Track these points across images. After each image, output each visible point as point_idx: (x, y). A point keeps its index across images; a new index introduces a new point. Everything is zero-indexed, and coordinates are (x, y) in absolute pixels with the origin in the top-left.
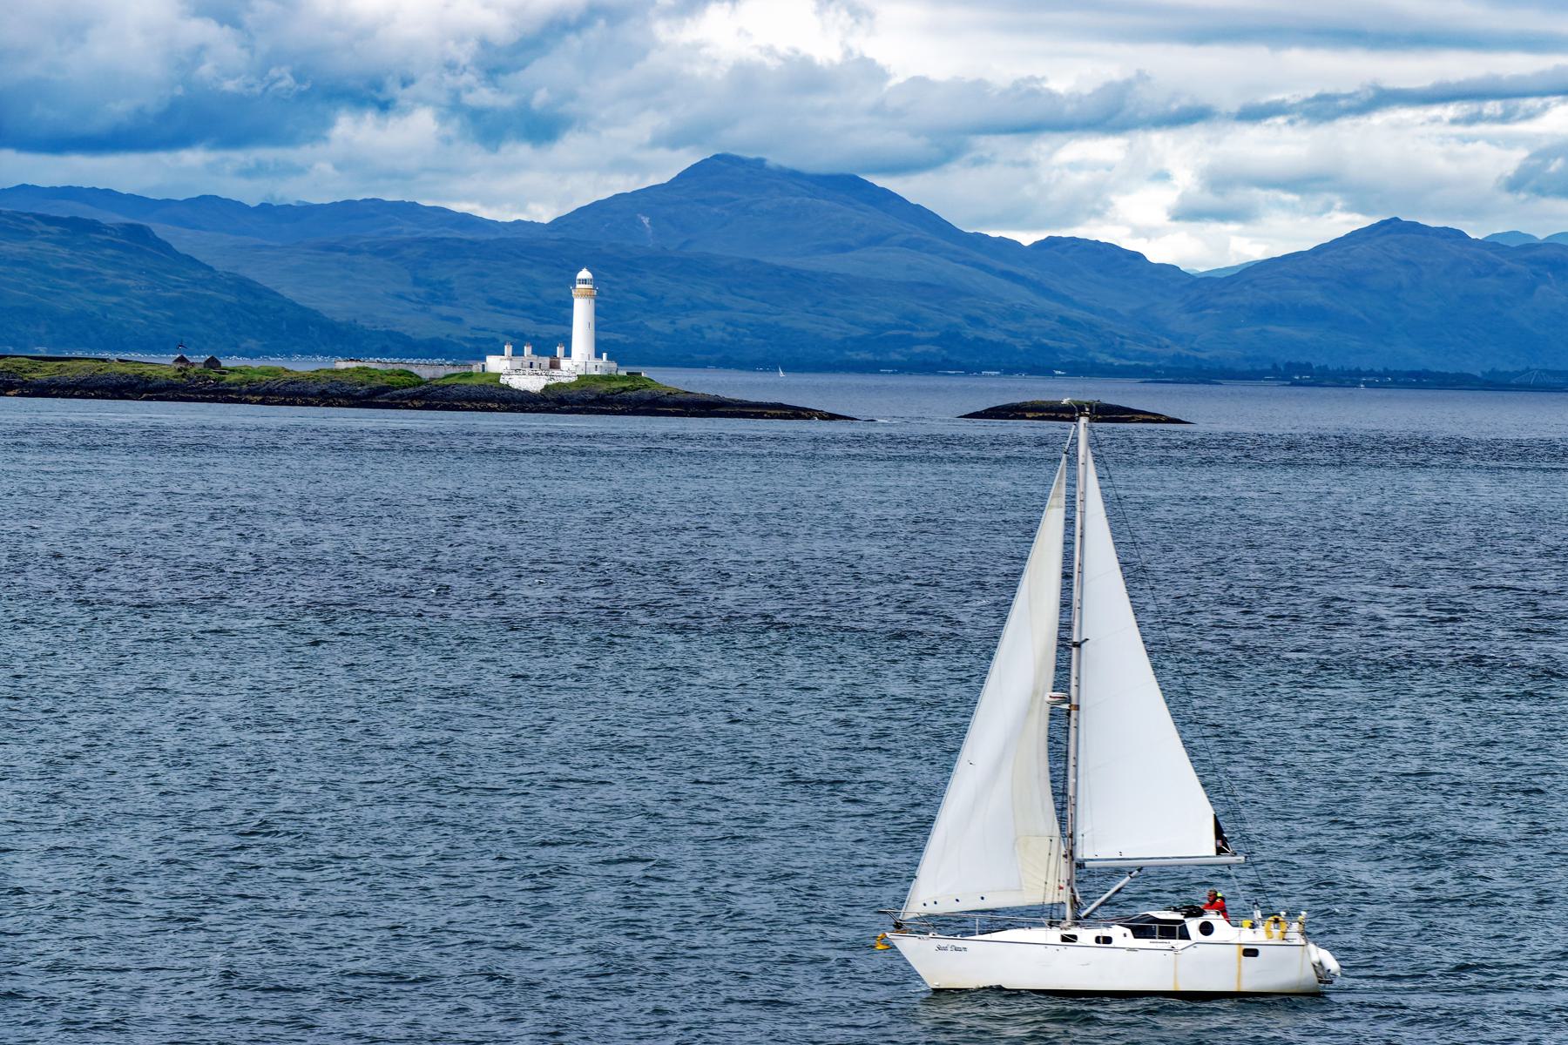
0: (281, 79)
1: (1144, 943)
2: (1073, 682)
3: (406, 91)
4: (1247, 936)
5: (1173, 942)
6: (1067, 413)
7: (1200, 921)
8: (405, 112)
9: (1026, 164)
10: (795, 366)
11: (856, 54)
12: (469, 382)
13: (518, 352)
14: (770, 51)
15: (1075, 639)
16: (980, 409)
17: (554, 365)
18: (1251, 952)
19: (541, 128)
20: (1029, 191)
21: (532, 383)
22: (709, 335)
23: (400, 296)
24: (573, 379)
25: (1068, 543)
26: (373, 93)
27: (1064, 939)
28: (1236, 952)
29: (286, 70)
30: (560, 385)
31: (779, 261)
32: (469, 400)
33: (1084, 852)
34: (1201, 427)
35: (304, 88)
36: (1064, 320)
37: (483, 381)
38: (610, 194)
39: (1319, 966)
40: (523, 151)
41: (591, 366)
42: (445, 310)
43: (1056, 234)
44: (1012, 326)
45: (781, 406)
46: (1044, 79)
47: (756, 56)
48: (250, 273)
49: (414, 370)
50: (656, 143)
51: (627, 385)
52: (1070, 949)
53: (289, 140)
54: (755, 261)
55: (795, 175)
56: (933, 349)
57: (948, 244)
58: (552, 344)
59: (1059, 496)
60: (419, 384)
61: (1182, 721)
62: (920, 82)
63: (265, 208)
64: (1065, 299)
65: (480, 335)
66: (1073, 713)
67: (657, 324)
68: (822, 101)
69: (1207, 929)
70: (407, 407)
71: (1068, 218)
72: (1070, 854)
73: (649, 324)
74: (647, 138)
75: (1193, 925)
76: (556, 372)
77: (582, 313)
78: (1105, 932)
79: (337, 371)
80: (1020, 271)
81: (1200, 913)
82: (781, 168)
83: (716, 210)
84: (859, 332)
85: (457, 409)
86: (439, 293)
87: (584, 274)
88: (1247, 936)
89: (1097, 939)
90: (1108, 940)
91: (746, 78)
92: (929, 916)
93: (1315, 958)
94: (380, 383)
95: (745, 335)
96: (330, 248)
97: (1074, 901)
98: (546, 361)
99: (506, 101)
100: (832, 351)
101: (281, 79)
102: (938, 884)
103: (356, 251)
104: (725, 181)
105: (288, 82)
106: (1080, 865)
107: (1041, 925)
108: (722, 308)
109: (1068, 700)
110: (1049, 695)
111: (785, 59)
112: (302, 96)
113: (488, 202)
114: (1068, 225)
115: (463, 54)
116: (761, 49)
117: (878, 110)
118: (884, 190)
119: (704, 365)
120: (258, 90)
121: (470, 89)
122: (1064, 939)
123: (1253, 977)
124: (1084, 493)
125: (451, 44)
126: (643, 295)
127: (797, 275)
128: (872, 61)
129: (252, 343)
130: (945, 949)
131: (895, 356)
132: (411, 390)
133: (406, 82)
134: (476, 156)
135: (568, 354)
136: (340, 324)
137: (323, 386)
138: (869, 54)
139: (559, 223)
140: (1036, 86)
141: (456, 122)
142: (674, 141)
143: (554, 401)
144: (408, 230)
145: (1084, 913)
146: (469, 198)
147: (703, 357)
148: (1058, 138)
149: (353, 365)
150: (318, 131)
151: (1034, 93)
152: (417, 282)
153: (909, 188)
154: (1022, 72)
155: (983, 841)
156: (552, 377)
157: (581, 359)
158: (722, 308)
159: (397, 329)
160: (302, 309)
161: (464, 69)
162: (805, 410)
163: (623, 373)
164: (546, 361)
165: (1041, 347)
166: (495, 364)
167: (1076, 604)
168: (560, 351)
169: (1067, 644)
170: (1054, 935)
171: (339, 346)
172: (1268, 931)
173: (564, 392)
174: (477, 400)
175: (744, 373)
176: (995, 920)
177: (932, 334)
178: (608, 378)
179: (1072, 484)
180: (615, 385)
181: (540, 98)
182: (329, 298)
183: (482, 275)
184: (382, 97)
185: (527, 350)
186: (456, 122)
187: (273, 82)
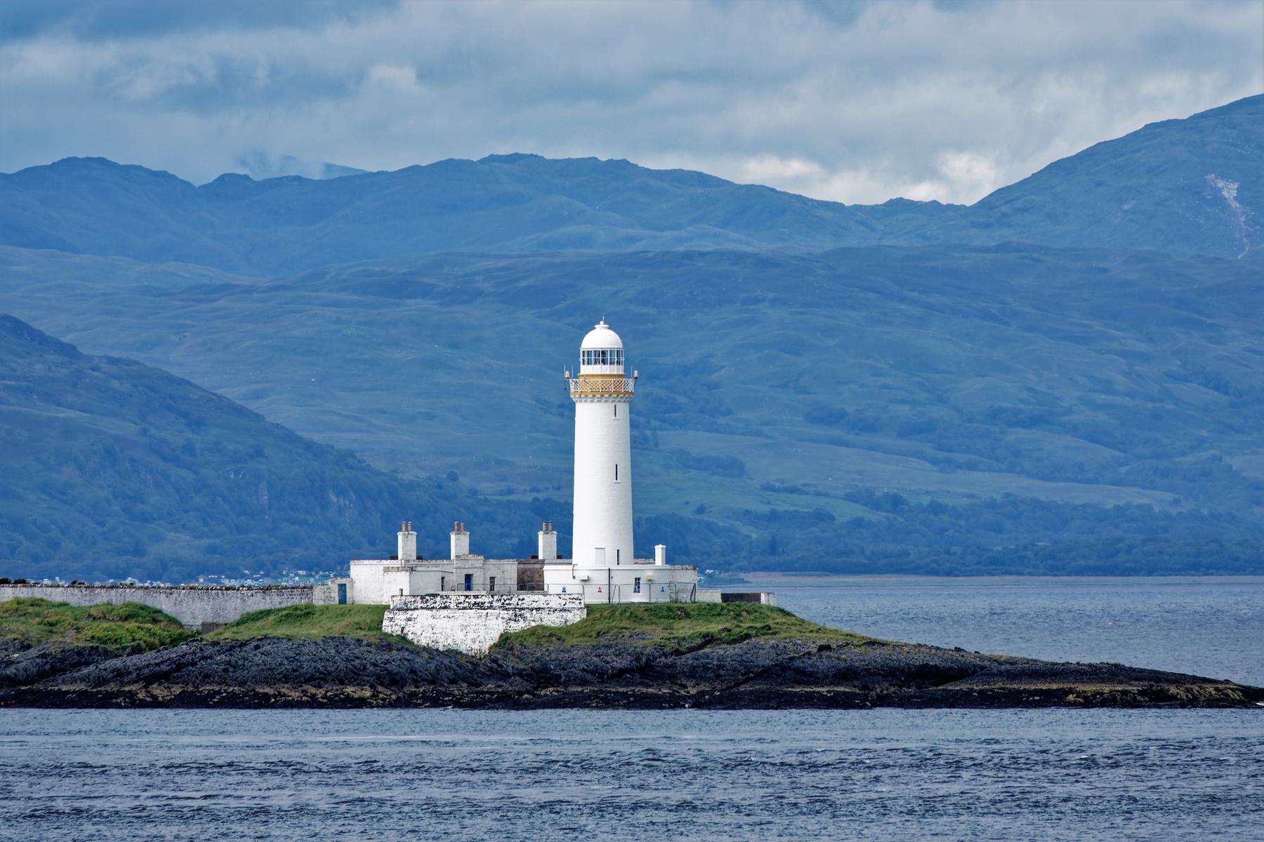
12: (301, 631)
13: (432, 550)
17: (530, 582)
21: (468, 630)
24: (575, 617)
37: (337, 627)
41: (624, 579)
45: (1115, 672)
48: (182, 360)
49: (164, 603)
51: (714, 627)
58: (529, 520)
60: (174, 642)
65: (782, 504)
70: (134, 703)
73: (1236, 462)
76: (530, 599)
77: (597, 435)
85: (262, 702)
87: (601, 337)
94: (72, 640)
98: (509, 570)
126: (1218, 384)
132: (149, 657)
135: (564, 553)
136: (411, 486)
139: (1002, 204)
143: (522, 677)
156: (518, 614)
157: (595, 562)
162: (1179, 679)
163: (714, 596)
164: (509, 570)
166: (373, 581)
168: (545, 543)
173: (549, 653)
174: (317, 678)
180: (686, 629)
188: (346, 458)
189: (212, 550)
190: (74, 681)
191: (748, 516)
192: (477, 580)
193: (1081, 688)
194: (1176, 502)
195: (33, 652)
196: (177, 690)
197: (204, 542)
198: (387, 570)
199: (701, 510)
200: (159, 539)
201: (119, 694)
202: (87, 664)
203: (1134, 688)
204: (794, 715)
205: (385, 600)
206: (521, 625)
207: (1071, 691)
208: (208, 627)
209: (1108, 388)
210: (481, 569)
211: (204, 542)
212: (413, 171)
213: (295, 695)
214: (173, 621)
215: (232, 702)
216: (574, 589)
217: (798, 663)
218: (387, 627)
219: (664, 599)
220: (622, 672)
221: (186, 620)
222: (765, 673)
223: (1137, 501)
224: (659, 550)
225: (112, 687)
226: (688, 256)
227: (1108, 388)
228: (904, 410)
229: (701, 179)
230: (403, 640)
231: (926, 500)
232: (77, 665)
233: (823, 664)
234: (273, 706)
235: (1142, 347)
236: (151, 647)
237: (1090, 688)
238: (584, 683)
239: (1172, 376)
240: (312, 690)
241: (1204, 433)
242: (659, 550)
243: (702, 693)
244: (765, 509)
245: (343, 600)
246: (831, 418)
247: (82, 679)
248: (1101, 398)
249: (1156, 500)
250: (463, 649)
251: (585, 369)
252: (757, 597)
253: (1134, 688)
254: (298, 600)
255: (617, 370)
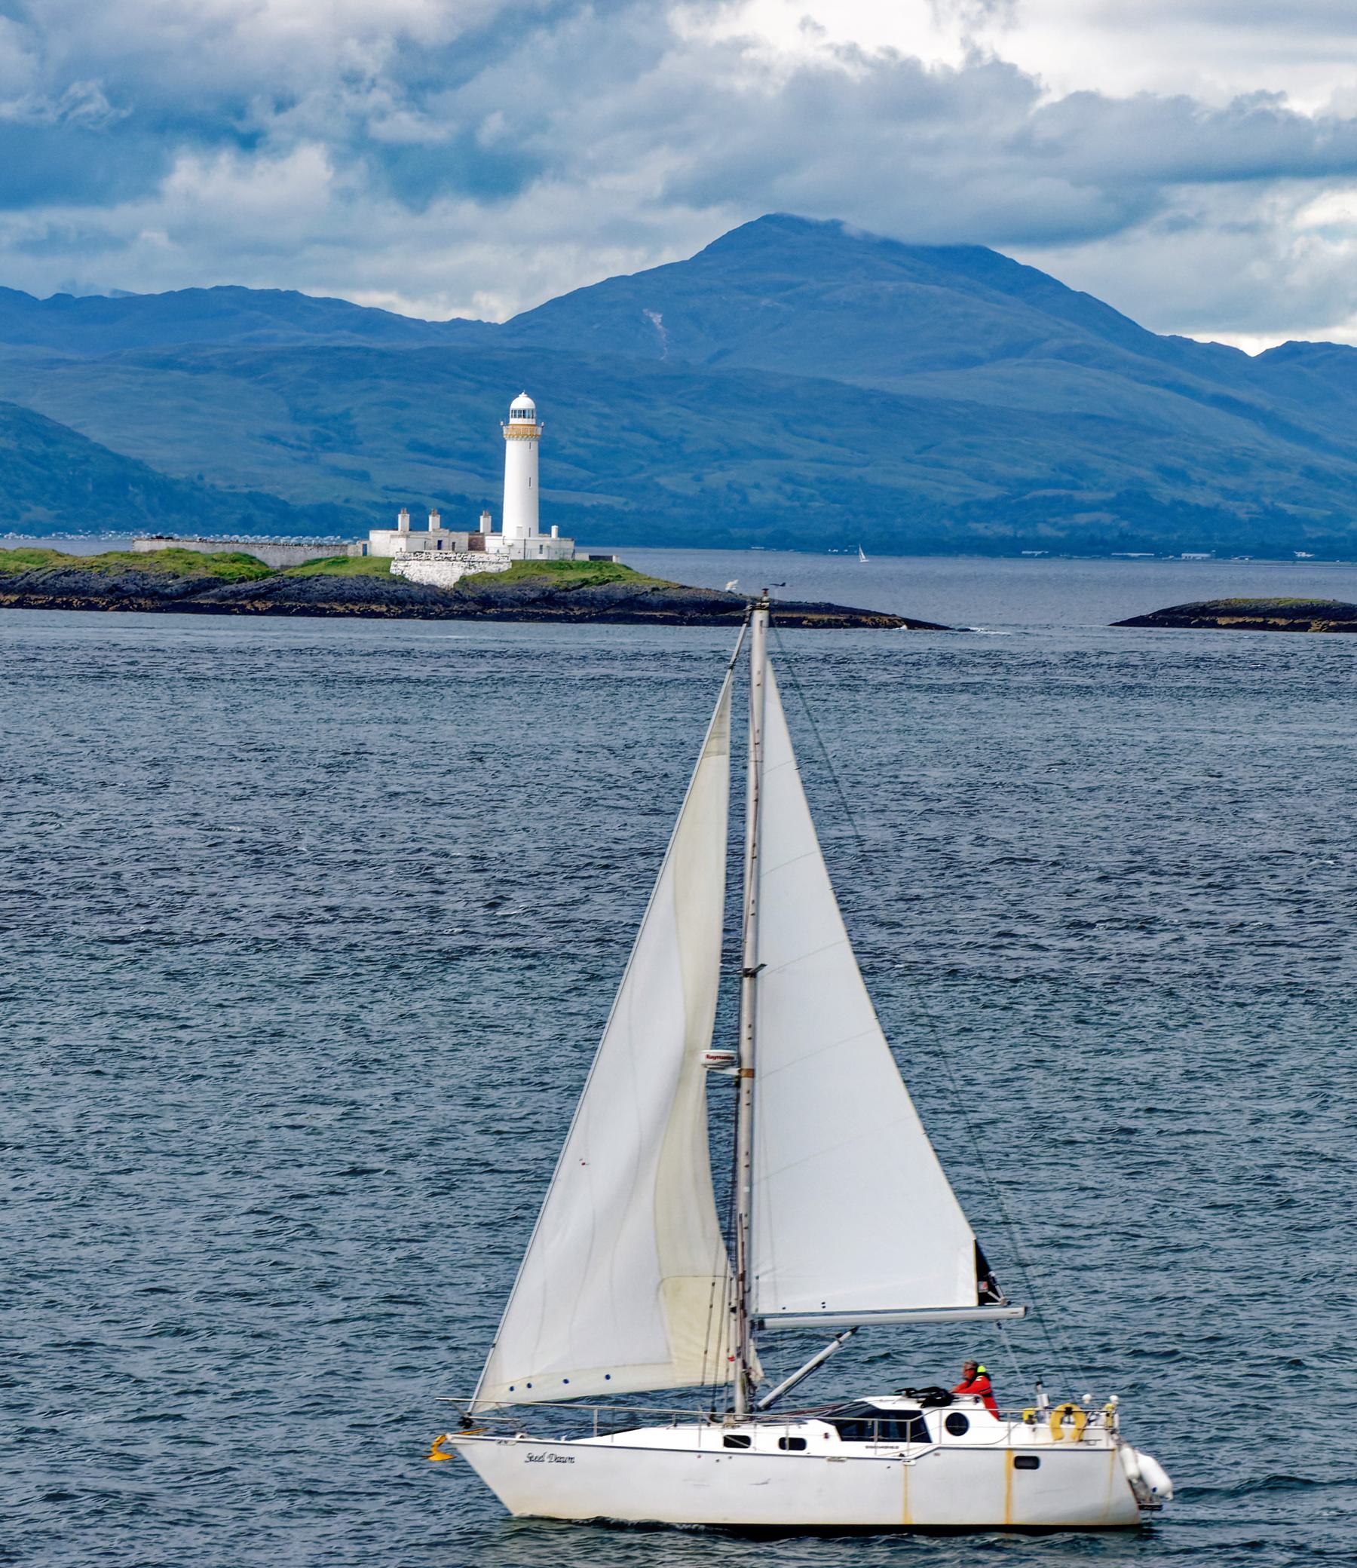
0: (87, 99)
1: (857, 1448)
2: (745, 1033)
3: (283, 118)
4: (1023, 1437)
5: (902, 1446)
6: (726, 611)
7: (947, 1412)
8: (281, 151)
9: (1252, 228)
10: (889, 545)
11: (987, 57)
12: (342, 571)
13: (419, 525)
14: (852, 52)
15: (748, 964)
16: (1146, 611)
17: (476, 545)
18: (1027, 1462)
19: (496, 176)
20: (1259, 271)
21: (439, 572)
22: (755, 497)
23: (272, 439)
25: (737, 812)
26: (233, 122)
27: (729, 1442)
28: (1004, 1460)
29: (93, 85)
30: (485, 576)
31: (865, 382)
32: (341, 599)
33: (763, 1304)
34: (990, 632)
35: (125, 114)
36: (1310, 472)
37: (363, 570)
38: (599, 278)
39: (1138, 1483)
40: (467, 211)
42: (343, 459)
43: (1299, 338)
44: (1232, 483)
45: (829, 608)
46: (1281, 95)
47: (827, 58)
48: (38, 402)
49: (258, 553)
50: (673, 196)
51: (588, 575)
52: (739, 1458)
53: (99, 196)
54: (823, 383)
55: (889, 247)
56: (1106, 518)
57: (1131, 355)
58: (471, 512)
59: (720, 735)
60: (265, 576)
61: (918, 1089)
62: (1086, 102)
63: (61, 302)
64: (1311, 439)
66: (745, 1082)
67: (674, 481)
68: (932, 131)
69: (957, 1425)
70: (244, 611)
71: (1322, 309)
72: (741, 1308)
73: (663, 481)
74: (658, 190)
75: (935, 1419)
77: (518, 461)
78: (795, 1431)
79: (137, 556)
80: (1244, 395)
81: (947, 1399)
82: (867, 236)
83: (765, 302)
84: (989, 492)
85: (322, 613)
86: (334, 433)
87: (522, 402)
88: (1023, 1437)
89: (782, 1443)
90: (798, 1444)
91: (813, 95)
92: (519, 1407)
93: (1132, 1470)
94: (202, 573)
95: (812, 498)
96: (167, 364)
97: (748, 1384)
98: (463, 538)
99: (439, 133)
100: (948, 523)
101: (87, 99)
102: (524, 1362)
103: (206, 368)
104: (778, 254)
105: (99, 104)
106: (759, 1324)
107: (693, 1420)
108: (775, 454)
109: (736, 1061)
110: (705, 1053)
111: (878, 67)
112: (120, 128)
113: (410, 290)
114: (1325, 324)
115: (371, 60)
116: (837, 51)
117: (1020, 144)
118: (1030, 271)
119: (747, 544)
120: (51, 117)
121: (382, 115)
122: (729, 1442)
123: (1032, 1501)
124: (761, 731)
125: (352, 45)
126: (652, 435)
127: (893, 404)
128: (1012, 69)
129: (40, 513)
130: (540, 1459)
131: (1045, 530)
132: (250, 585)
133: (282, 105)
134: (390, 217)
135: (497, 528)
136: (176, 482)
137: (113, 578)
138: (1007, 58)
139: (521, 323)
140: (1269, 107)
141: (361, 164)
142: (700, 194)
144: (284, 335)
145: (762, 1403)
146: (382, 284)
147: (745, 532)
148: (1305, 187)
149: (162, 545)
150: (146, 180)
151: (1266, 118)
152: (297, 415)
153: (1069, 266)
154: (1248, 83)
155: (595, 1289)
157: (515, 535)
158: (775, 454)
159: (266, 489)
160: (120, 459)
161: (374, 83)
162: (867, 613)
165: (1277, 515)
166: (383, 543)
167: (749, 908)
168: (485, 523)
169: (736, 970)
170: (712, 1437)
171: (176, 517)
172: (1054, 1429)
173: (487, 587)
174: (353, 600)
175: (951, 560)
176: (627, 1411)
177: (1101, 496)
178: (561, 566)
179: (741, 723)
180: (571, 576)
181: (492, 129)
182: (165, 447)
183: (402, 405)
184: (244, 127)
185: (434, 521)
186: (361, 164)
187: (77, 103)
188: (137, 464)
189: (58, 517)
190: (208, 597)
191: (375, 505)
192: (445, 543)
193: (810, 617)
194: (626, 503)
195: (181, 580)
196: (270, 604)
197: (55, 512)
198: (392, 536)
199: (347, 501)
200: (29, 510)
201: (236, 606)
202: (213, 588)
203: (842, 618)
204: (641, 627)
205: (391, 554)
206: (473, 571)
207: (805, 619)
208: (284, 567)
209: (587, 435)
210: (444, 534)
211: (55, 512)
212: (170, 294)
213: (341, 609)
214: (262, 563)
215: (304, 612)
216: (504, 551)
217: (641, 598)
218: (393, 570)
219: (556, 558)
220: (534, 600)
221: (270, 563)
222: (621, 603)
223: (605, 502)
224: (554, 529)
225: (230, 602)
226: (338, 349)
227: (587, 435)
228: (464, 445)
229: (341, 303)
230: (402, 579)
231: (480, 498)
232: (207, 589)
233: (654, 599)
234: (328, 616)
235: (607, 410)
236: (251, 579)
237: (816, 617)
238: (512, 606)
239: (623, 428)
240: (351, 607)
241: (642, 463)
242: (554, 529)
243: (584, 614)
244: (386, 501)
245: (365, 553)
246: (424, 448)
247: (213, 596)
248: (582, 440)
249: (616, 501)
250: (438, 584)
251: (513, 421)
252: (610, 558)
253: (842, 618)
254: (338, 553)
255: (532, 421)
